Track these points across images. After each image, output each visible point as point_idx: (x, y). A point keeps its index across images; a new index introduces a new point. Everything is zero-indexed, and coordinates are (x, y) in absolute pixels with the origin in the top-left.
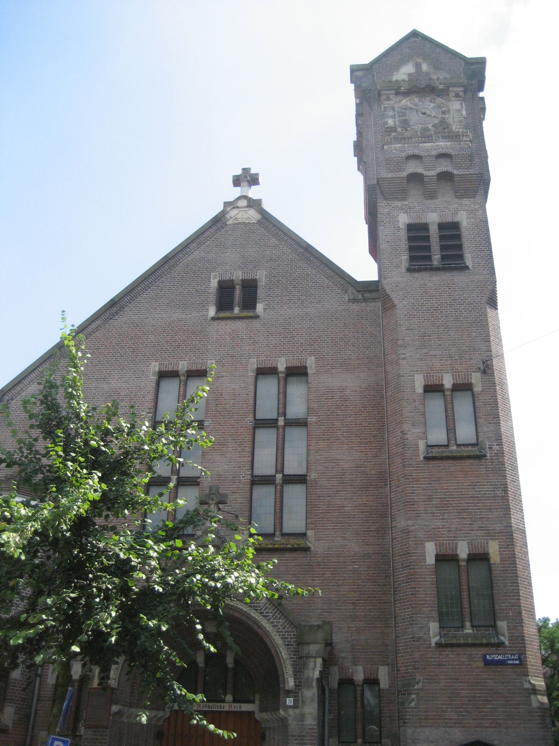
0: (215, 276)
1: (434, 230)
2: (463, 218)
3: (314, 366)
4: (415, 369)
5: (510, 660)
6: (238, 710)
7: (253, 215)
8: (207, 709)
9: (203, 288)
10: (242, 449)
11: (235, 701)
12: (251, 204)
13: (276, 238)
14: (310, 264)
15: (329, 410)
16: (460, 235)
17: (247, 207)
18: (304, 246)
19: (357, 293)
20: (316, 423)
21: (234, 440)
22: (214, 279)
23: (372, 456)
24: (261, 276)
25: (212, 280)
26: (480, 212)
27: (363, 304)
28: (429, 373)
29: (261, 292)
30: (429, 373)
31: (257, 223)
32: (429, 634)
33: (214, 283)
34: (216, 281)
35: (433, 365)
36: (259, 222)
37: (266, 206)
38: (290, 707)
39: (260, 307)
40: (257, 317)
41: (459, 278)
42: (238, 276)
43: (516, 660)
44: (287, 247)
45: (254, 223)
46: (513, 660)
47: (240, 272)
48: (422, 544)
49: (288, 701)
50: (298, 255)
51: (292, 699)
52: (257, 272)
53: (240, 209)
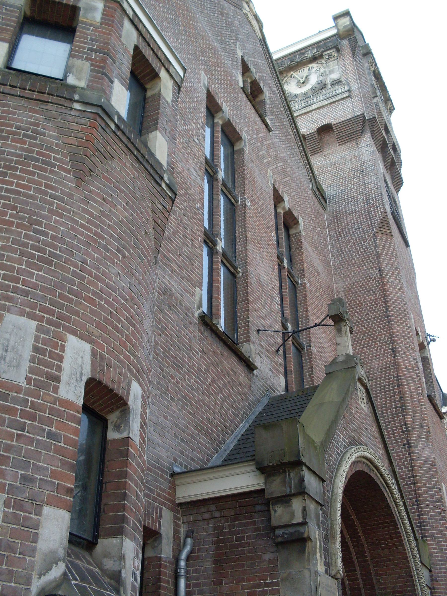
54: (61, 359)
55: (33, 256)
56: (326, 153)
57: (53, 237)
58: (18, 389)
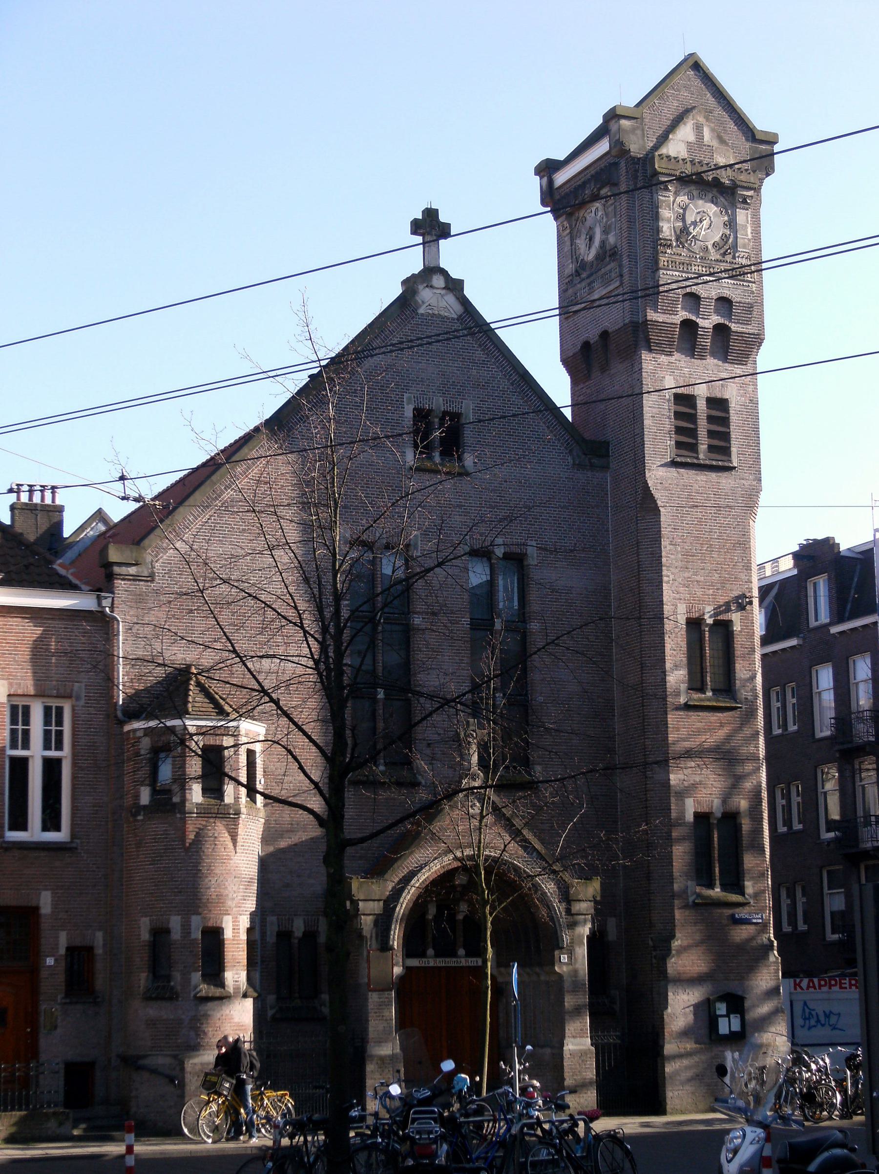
0: (409, 399)
1: (701, 405)
2: (732, 393)
3: (535, 555)
4: (677, 596)
5: (755, 919)
6: (475, 964)
7: (449, 305)
8: (444, 965)
9: (395, 417)
10: (460, 660)
11: (437, 955)
12: (450, 286)
13: (483, 350)
14: (526, 402)
15: (553, 617)
16: (728, 418)
17: (444, 288)
18: (521, 372)
19: (584, 456)
20: (540, 632)
21: (450, 646)
22: (408, 404)
23: (600, 680)
24: (468, 408)
25: (405, 406)
26: (751, 388)
27: (589, 474)
28: (691, 603)
29: (469, 435)
30: (691, 603)
31: (458, 319)
32: (687, 893)
33: (409, 411)
34: (411, 407)
35: (695, 594)
36: (460, 318)
37: (469, 292)
38: (565, 964)
39: (469, 460)
40: (464, 473)
41: (725, 481)
42: (438, 403)
43: (759, 918)
44: (498, 367)
45: (453, 319)
46: (757, 918)
47: (441, 399)
48: (682, 800)
49: (48, 961)
50: (512, 384)
51: (566, 956)
52: (462, 403)
53: (435, 291)
54: (190, 925)
55: (175, 892)
56: (612, 372)
57: (181, 881)
58: (178, 940)
